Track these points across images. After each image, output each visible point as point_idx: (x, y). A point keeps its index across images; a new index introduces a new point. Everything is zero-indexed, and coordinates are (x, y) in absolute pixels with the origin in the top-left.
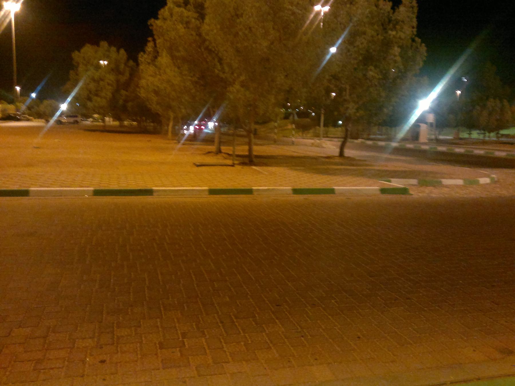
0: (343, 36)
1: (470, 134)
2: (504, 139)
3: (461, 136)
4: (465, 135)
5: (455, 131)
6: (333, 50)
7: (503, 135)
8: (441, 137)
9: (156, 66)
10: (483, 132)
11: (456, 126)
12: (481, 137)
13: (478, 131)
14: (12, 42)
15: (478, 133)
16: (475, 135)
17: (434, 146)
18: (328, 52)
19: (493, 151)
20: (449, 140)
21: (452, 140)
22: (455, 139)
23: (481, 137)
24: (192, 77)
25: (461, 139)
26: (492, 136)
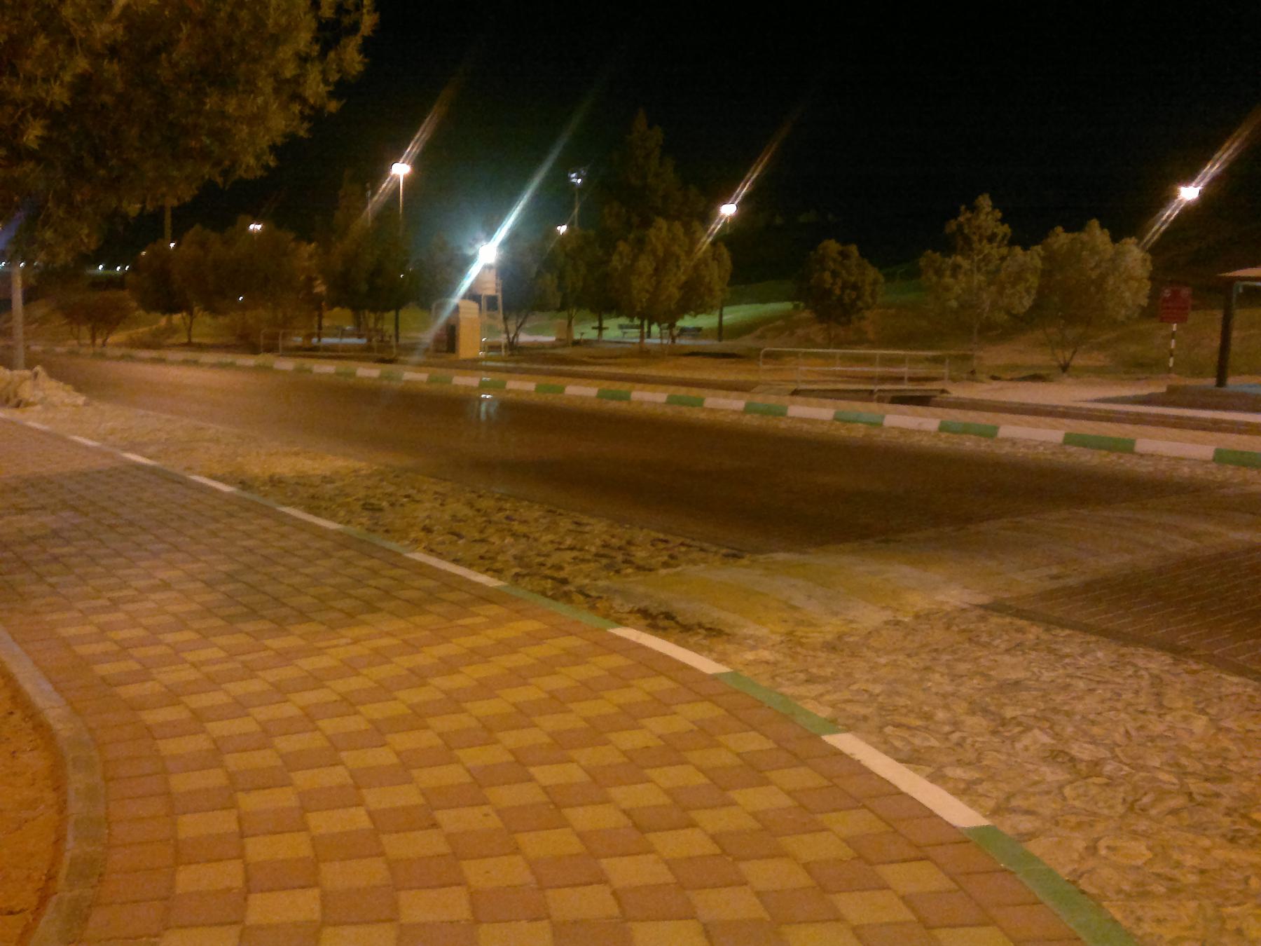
0: (754, 175)
1: (600, 329)
2: (684, 342)
3: (577, 337)
4: (585, 331)
5: (561, 320)
6: (1189, 193)
7: (683, 331)
8: (524, 338)
9: (1198, 940)
10: (637, 322)
11: (563, 307)
12: (633, 335)
13: (623, 321)
14: (1236, 268)
15: (621, 327)
16: (614, 329)
17: (1218, 675)
18: (1171, 196)
19: (695, 392)
20: (542, 346)
21: (553, 346)
22: (561, 343)
23: (633, 335)
24: (976, 741)
25: (577, 343)
26: (656, 336)
